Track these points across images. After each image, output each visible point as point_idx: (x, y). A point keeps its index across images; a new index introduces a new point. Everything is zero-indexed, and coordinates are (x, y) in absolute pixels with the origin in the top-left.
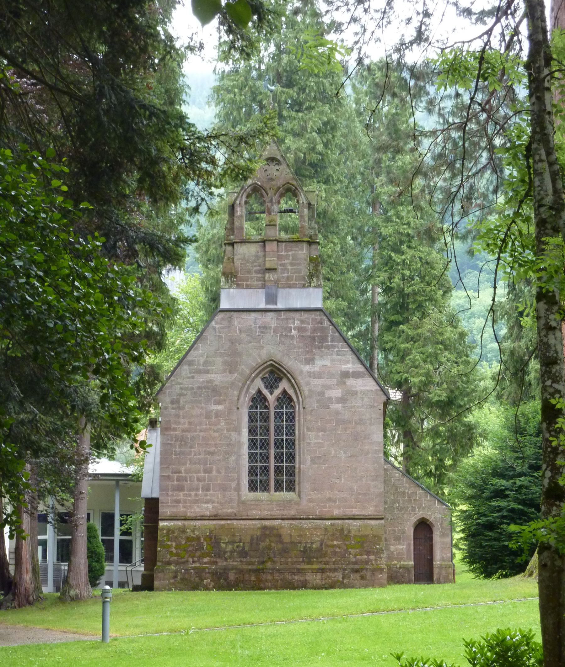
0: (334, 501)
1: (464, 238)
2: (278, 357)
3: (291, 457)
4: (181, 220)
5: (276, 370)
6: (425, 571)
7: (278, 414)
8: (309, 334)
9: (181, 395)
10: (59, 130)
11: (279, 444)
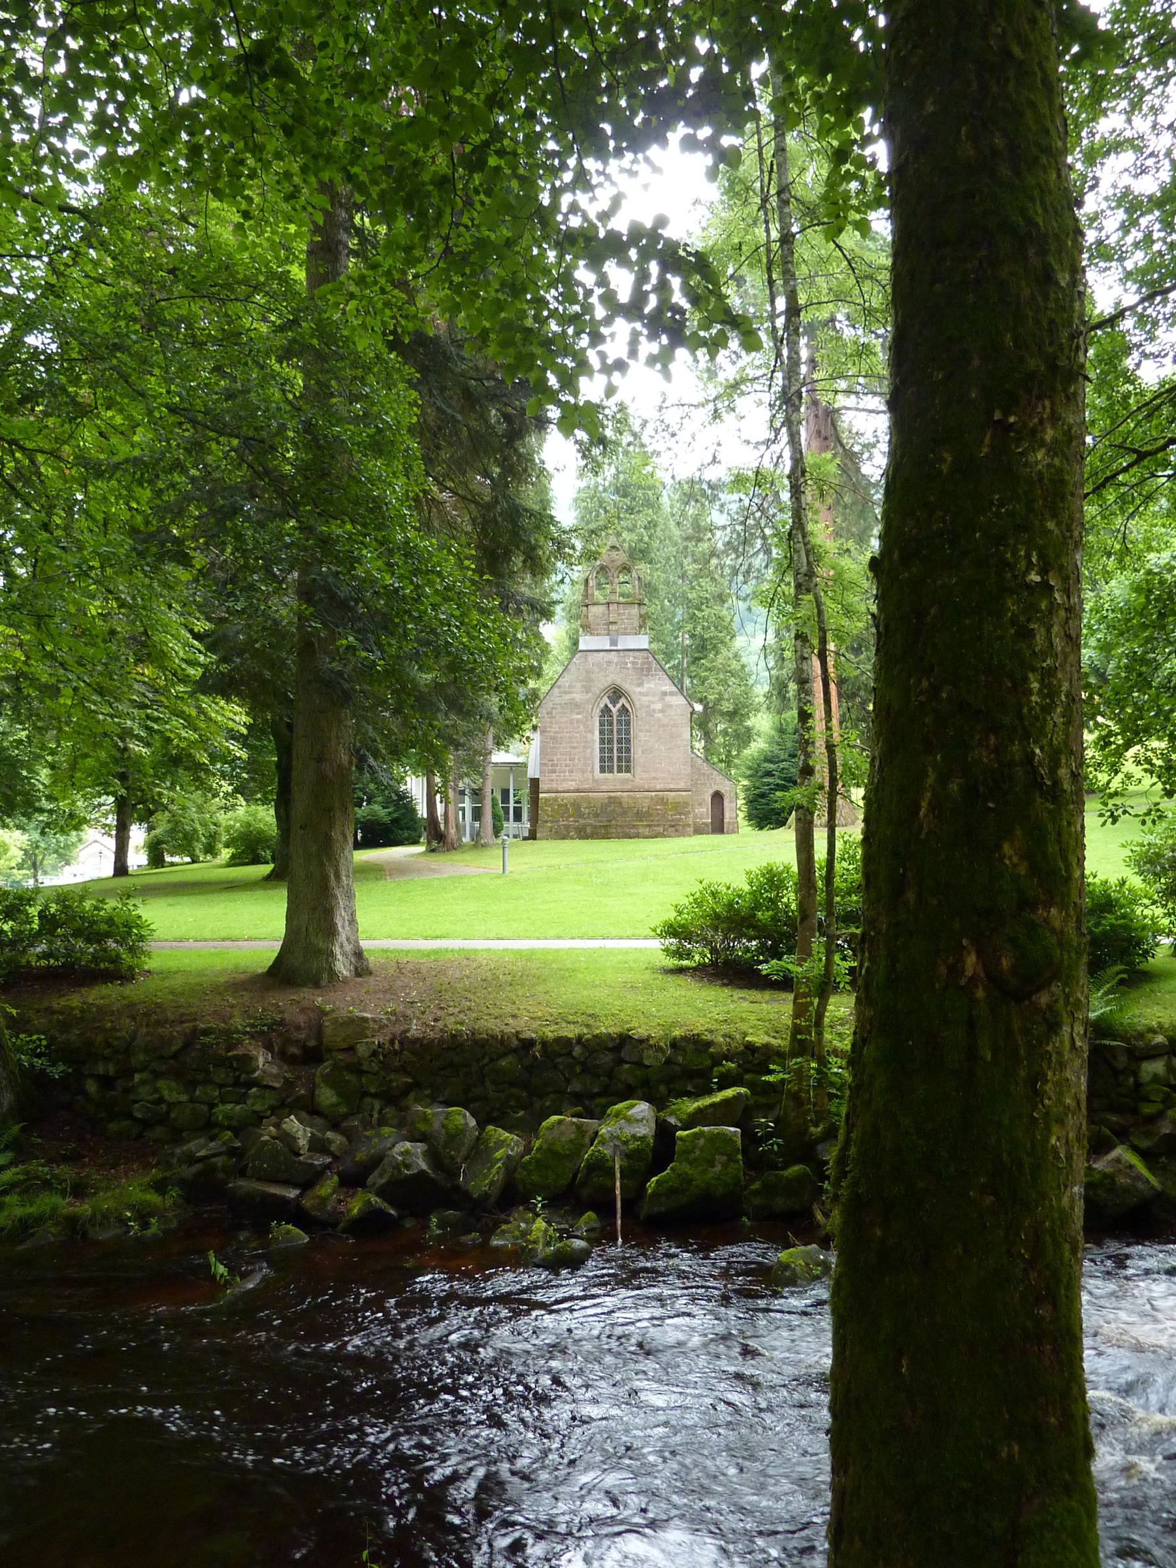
1: (745, 599)
2: (619, 682)
3: (628, 750)
4: (552, 590)
6: (718, 826)
10: (469, 528)
11: (619, 741)
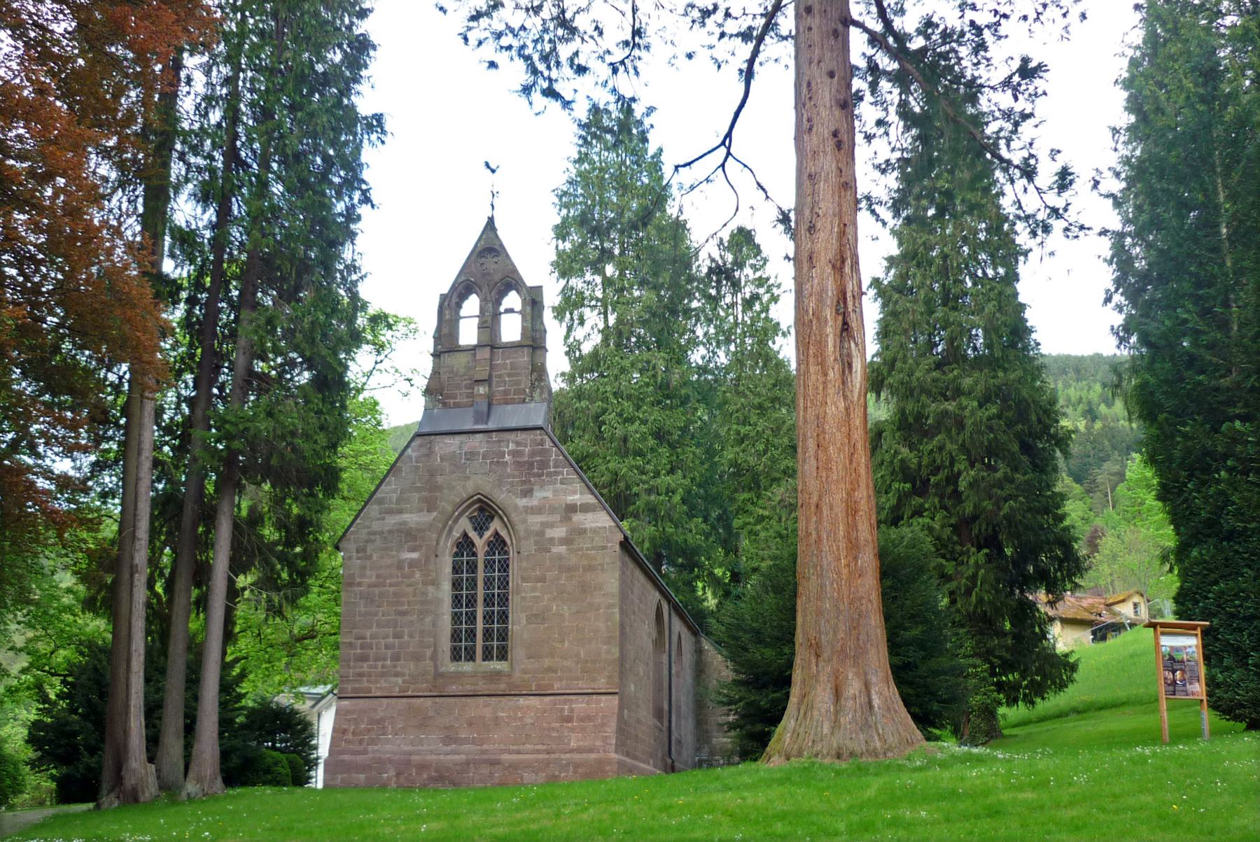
0: (555, 672)
3: (504, 617)
9: (367, 541)
11: (488, 601)
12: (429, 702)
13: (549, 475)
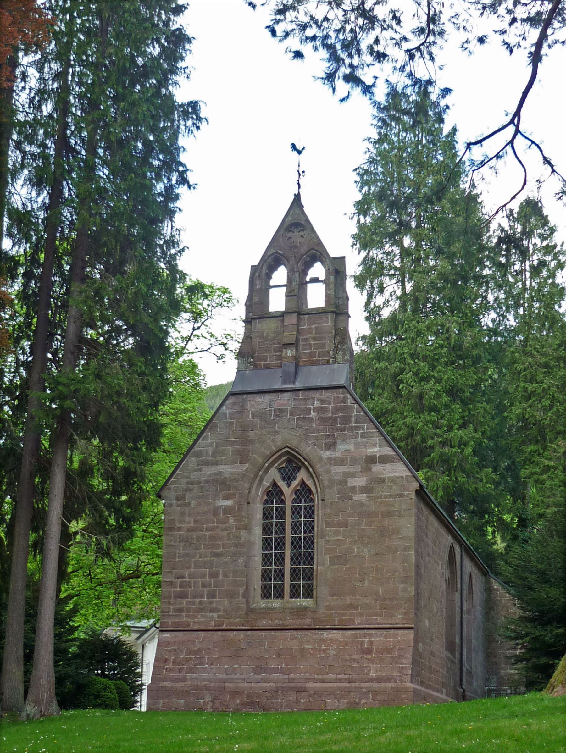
0: (356, 608)
2: (294, 443)
3: (310, 558)
5: (292, 458)
7: (296, 509)
8: (330, 415)
9: (186, 490)
11: (295, 544)
12: (242, 635)
13: (351, 429)
